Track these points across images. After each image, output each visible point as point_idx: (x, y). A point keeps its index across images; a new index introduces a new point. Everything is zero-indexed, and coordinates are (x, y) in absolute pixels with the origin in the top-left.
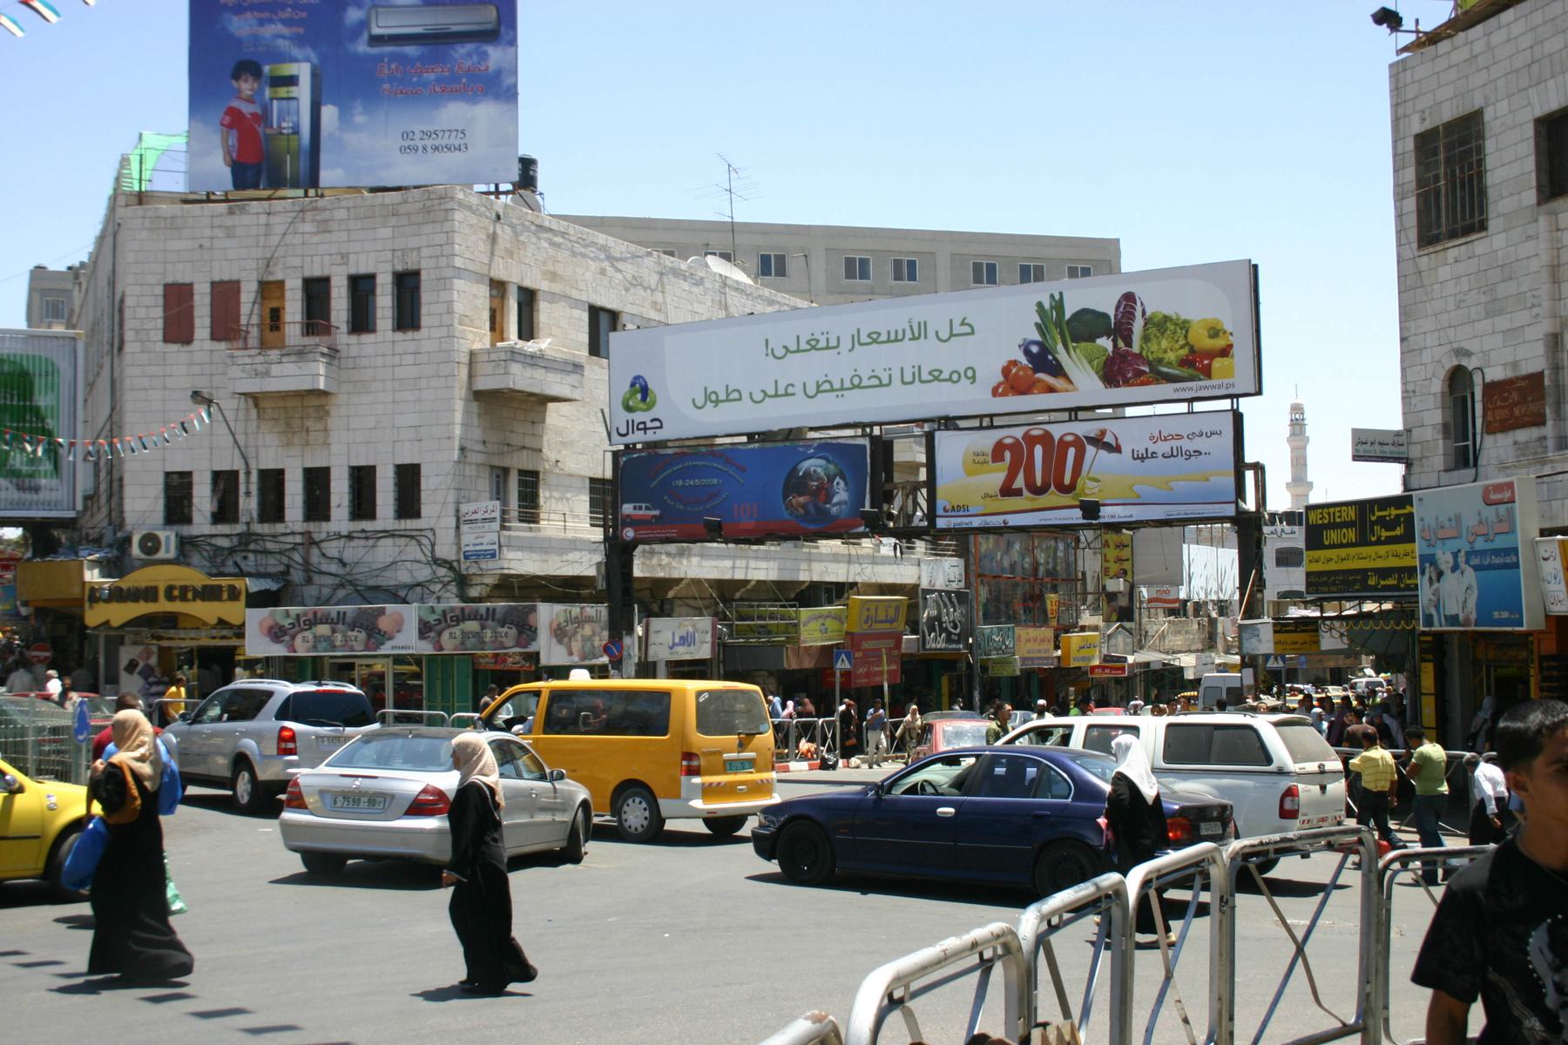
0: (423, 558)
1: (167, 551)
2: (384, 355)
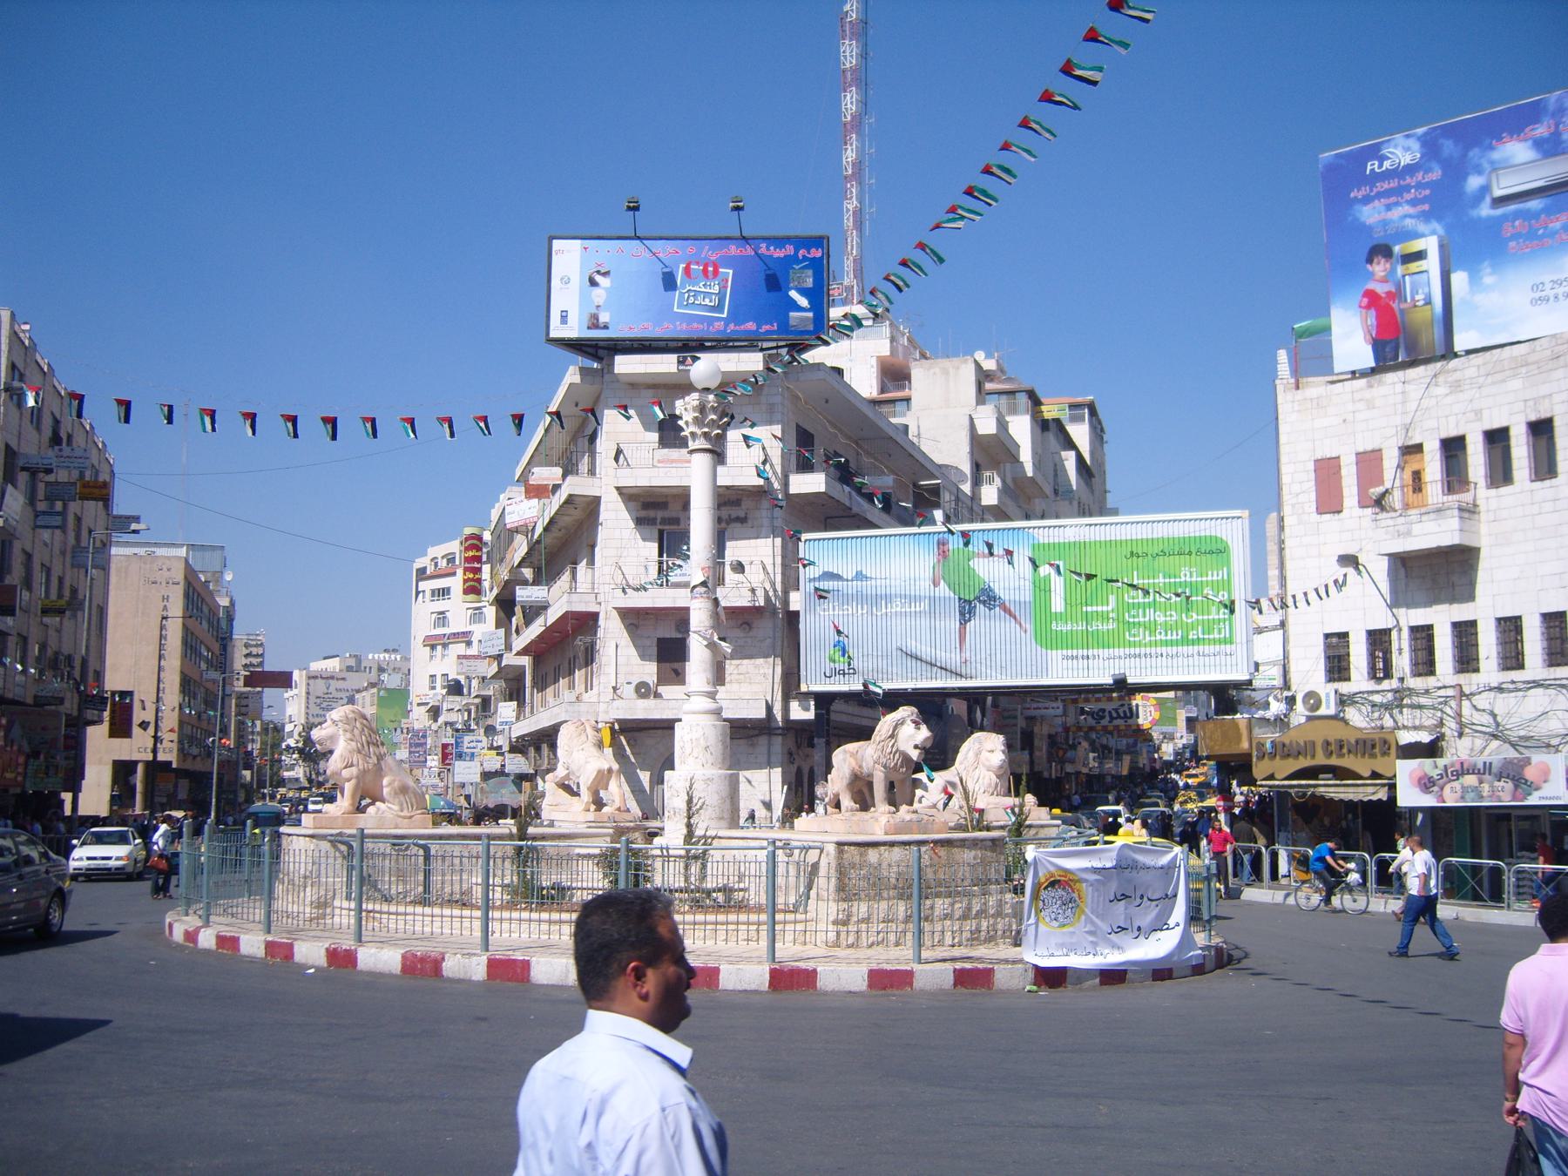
1: (1328, 707)
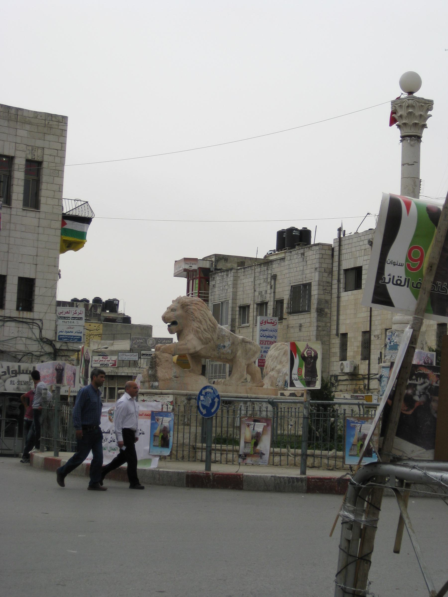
0: (34, 337)
2: (17, 208)
